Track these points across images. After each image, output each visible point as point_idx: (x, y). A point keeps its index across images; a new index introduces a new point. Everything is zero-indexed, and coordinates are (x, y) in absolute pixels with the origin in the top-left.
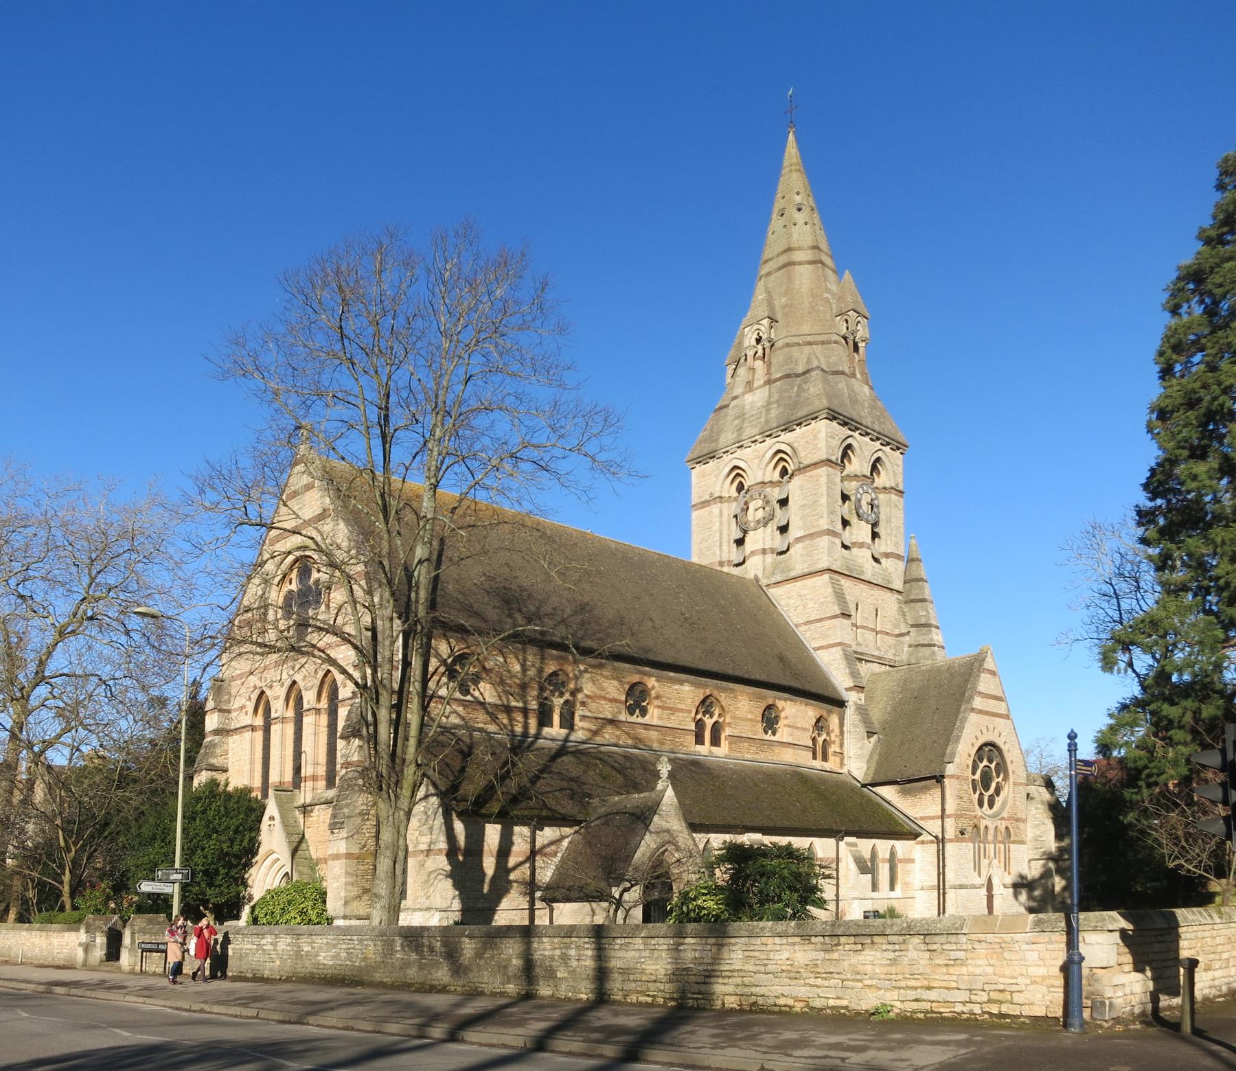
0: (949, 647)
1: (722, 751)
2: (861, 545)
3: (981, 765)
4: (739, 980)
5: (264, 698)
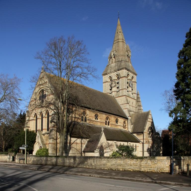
0: (144, 110)
1: (109, 126)
2: (130, 91)
3: (149, 131)
4: (122, 166)
5: (36, 115)
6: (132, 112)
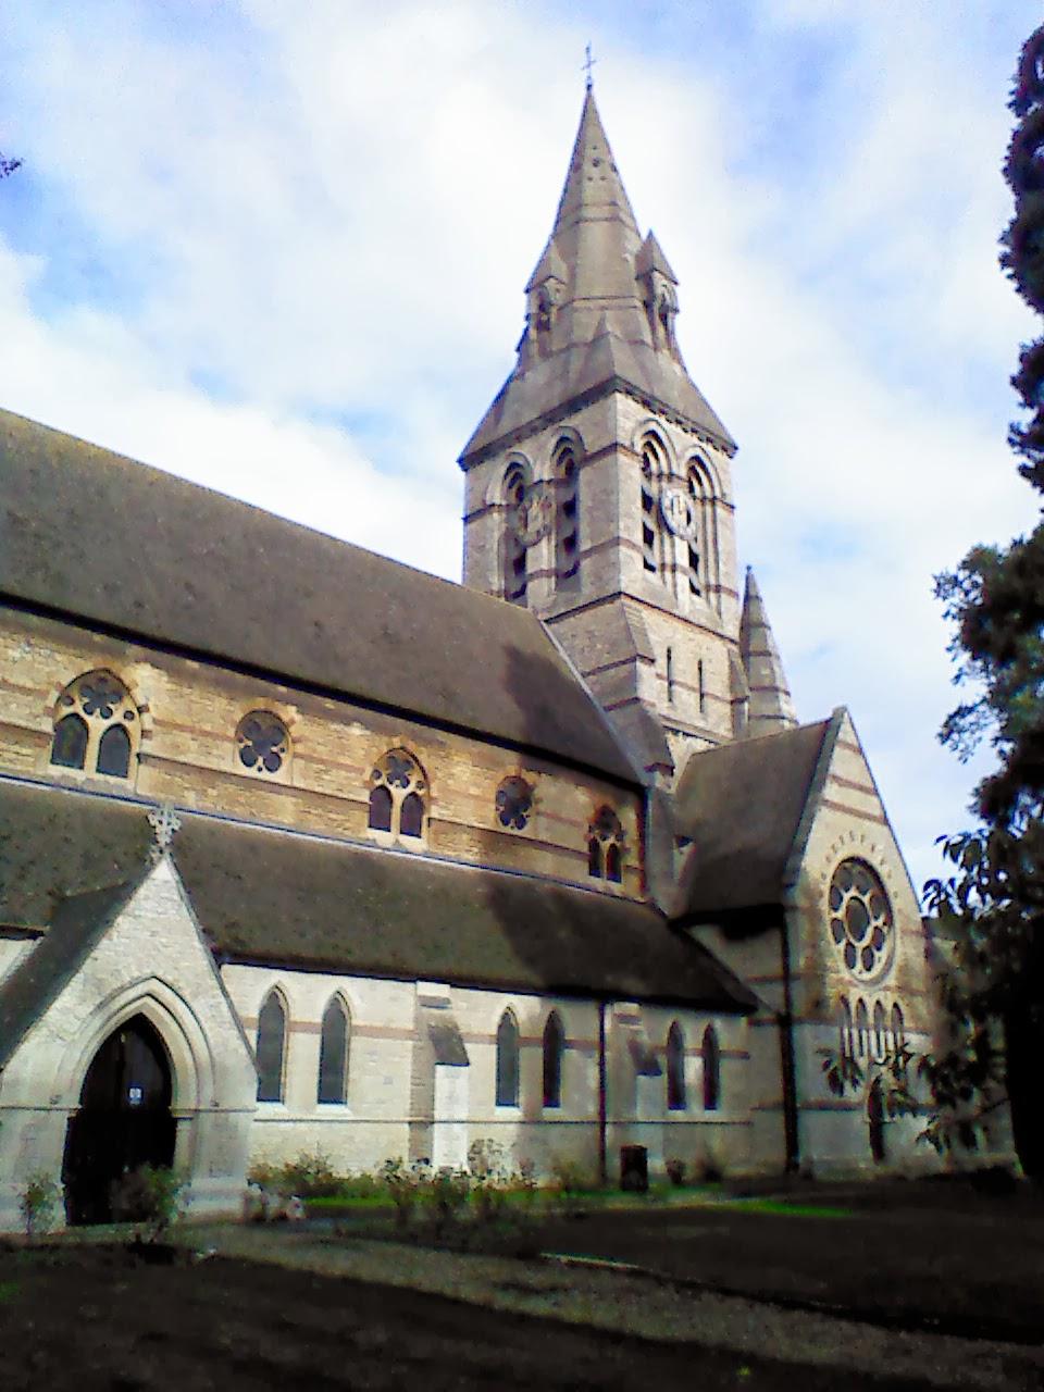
3: (847, 896)
6: (689, 739)
